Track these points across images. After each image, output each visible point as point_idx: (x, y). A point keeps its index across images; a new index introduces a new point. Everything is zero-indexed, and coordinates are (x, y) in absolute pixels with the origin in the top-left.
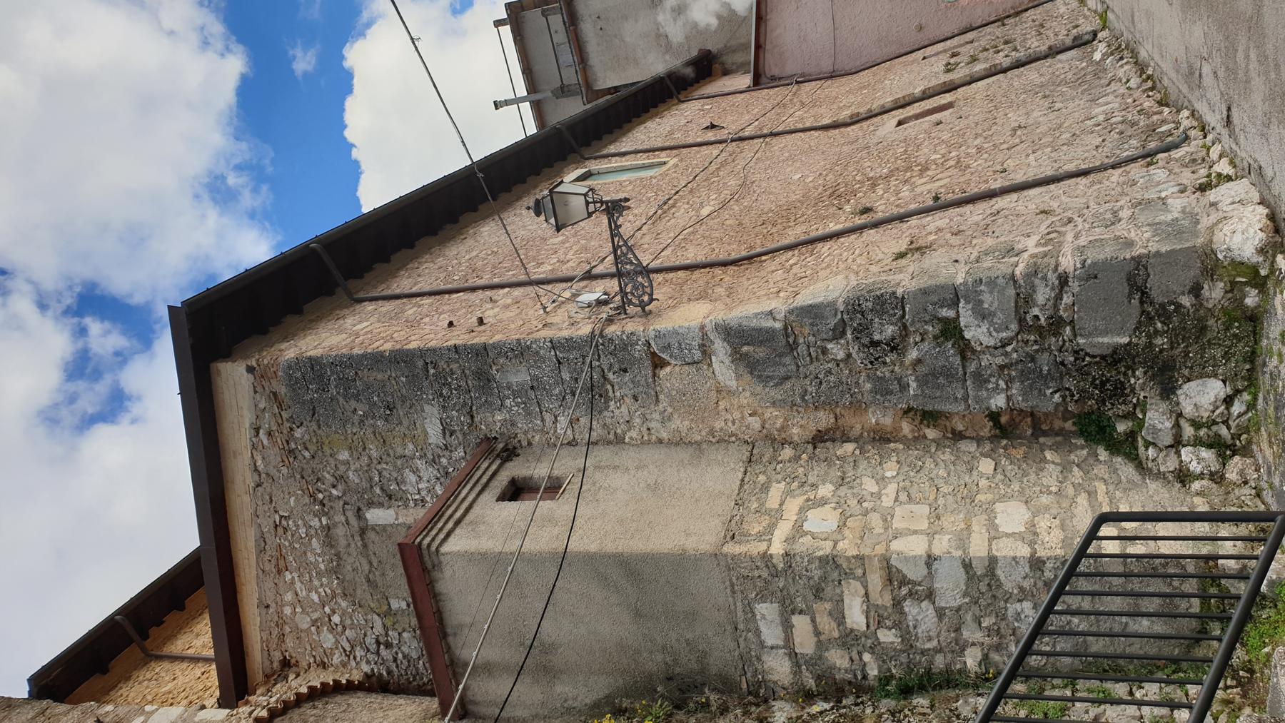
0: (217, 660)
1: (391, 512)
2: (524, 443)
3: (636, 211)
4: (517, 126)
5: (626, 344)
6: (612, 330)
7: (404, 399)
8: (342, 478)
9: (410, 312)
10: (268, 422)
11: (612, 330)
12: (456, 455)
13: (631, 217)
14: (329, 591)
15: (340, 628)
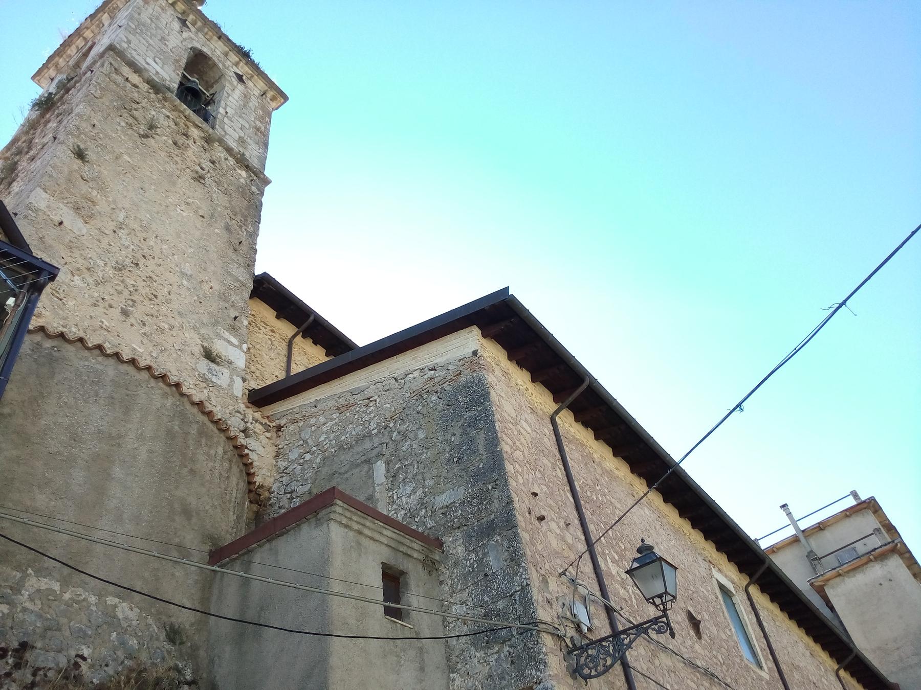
0: (677, 464)
1: (384, 480)
2: (441, 578)
3: (697, 647)
4: (761, 526)
5: (535, 659)
6: (547, 641)
7: (466, 470)
8: (404, 436)
9: (546, 461)
10: (440, 374)
11: (547, 641)
12: (428, 520)
13: (689, 643)
14: (326, 447)
15: (302, 461)
